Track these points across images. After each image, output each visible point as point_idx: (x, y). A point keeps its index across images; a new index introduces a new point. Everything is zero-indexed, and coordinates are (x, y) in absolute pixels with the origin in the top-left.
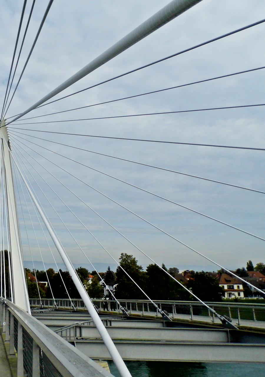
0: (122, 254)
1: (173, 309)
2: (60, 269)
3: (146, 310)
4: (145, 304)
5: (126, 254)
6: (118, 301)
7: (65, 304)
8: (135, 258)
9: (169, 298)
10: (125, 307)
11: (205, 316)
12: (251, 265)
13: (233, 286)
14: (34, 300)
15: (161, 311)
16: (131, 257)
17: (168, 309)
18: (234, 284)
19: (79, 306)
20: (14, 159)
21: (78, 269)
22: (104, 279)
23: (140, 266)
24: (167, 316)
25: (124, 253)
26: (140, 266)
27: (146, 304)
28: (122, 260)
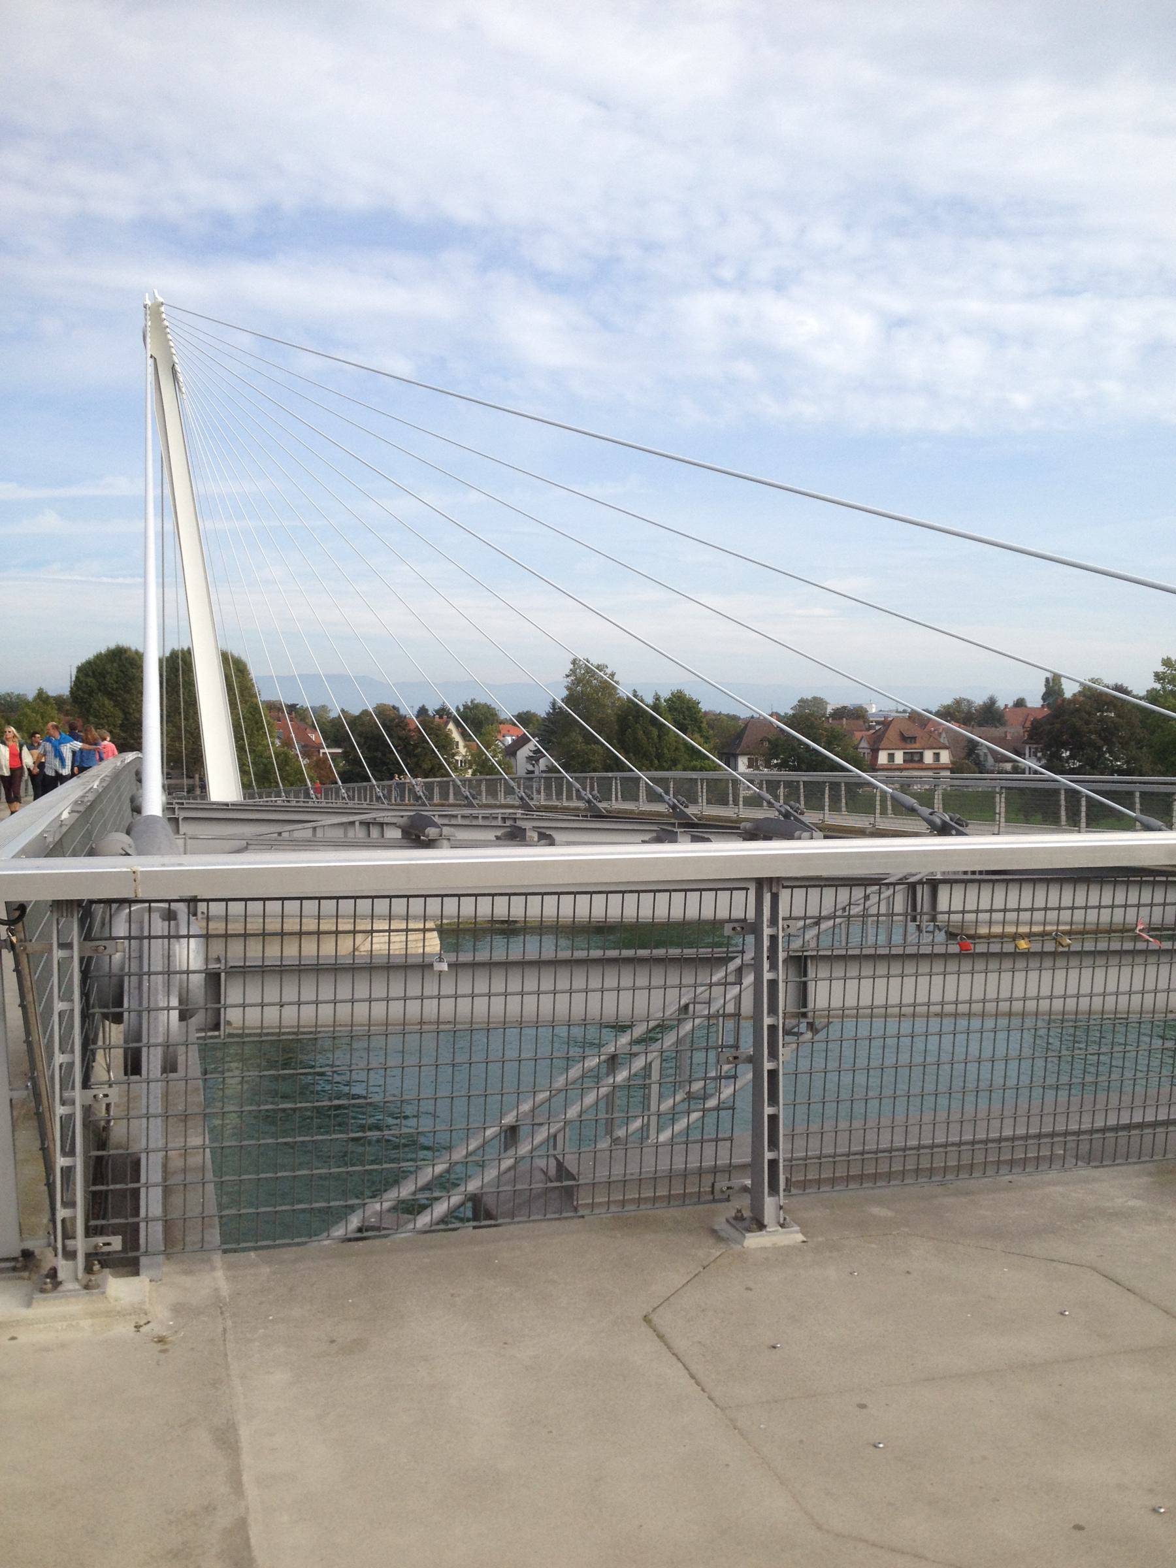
0: (574, 662)
2: (424, 706)
3: (835, 807)
4: (835, 786)
12: (1056, 688)
13: (921, 754)
18: (924, 749)
20: (450, 813)
21: (466, 707)
22: (537, 739)
27: (838, 784)
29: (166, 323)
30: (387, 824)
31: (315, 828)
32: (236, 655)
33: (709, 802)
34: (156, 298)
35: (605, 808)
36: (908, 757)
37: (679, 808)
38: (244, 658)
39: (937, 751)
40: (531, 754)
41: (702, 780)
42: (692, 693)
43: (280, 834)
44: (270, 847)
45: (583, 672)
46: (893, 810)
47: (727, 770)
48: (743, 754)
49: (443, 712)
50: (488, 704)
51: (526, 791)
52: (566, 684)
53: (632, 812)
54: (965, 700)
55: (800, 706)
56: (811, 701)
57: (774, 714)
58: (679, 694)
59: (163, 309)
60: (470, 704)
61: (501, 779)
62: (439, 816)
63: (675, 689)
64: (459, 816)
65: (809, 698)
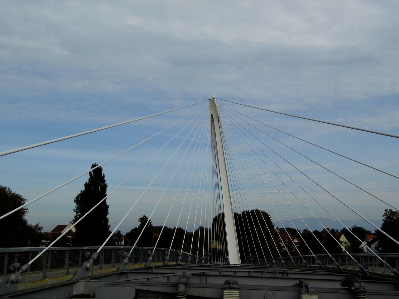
0: (386, 210)
21: (353, 228)
30: (289, 273)
31: (168, 277)
32: (262, 210)
38: (267, 211)
40: (376, 246)
43: (148, 279)
44: (113, 285)
45: (390, 214)
50: (361, 227)
52: (383, 219)
53: (351, 270)
59: (215, 99)
60: (354, 227)
62: (254, 271)
64: (265, 272)
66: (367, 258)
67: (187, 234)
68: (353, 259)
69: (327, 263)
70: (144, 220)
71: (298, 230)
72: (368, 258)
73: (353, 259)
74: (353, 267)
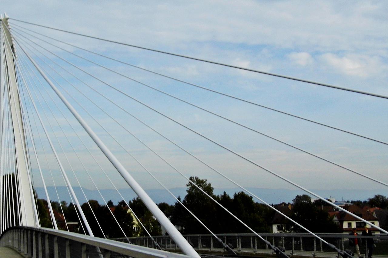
1: (199, 241)
2: (110, 201)
3: (298, 248)
5: (197, 178)
6: (128, 239)
7: (147, 242)
8: (210, 185)
9: (112, 236)
10: (159, 243)
11: (248, 248)
14: (227, 237)
15: (225, 245)
16: (205, 182)
17: (232, 241)
19: (254, 247)
23: (217, 195)
24: (283, 253)
25: (194, 176)
26: (217, 195)
28: (190, 186)
29: (10, 27)
33: (242, 247)
34: (5, 16)
35: (236, 252)
36: (358, 225)
37: (280, 252)
39: (350, 222)
41: (238, 237)
42: (248, 193)
46: (323, 249)
47: (309, 232)
48: (275, 223)
49: (123, 203)
51: (347, 250)
54: (380, 196)
55: (297, 199)
56: (302, 196)
57: (272, 205)
58: (242, 194)
59: (8, 21)
60: (136, 199)
61: (210, 237)
63: (240, 191)
65: (301, 195)
66: (250, 238)
67: (52, 202)
68: (327, 243)
69: (256, 248)
70: (225, 193)
71: (272, 205)
72: (212, 238)
73: (327, 243)
74: (254, 250)
